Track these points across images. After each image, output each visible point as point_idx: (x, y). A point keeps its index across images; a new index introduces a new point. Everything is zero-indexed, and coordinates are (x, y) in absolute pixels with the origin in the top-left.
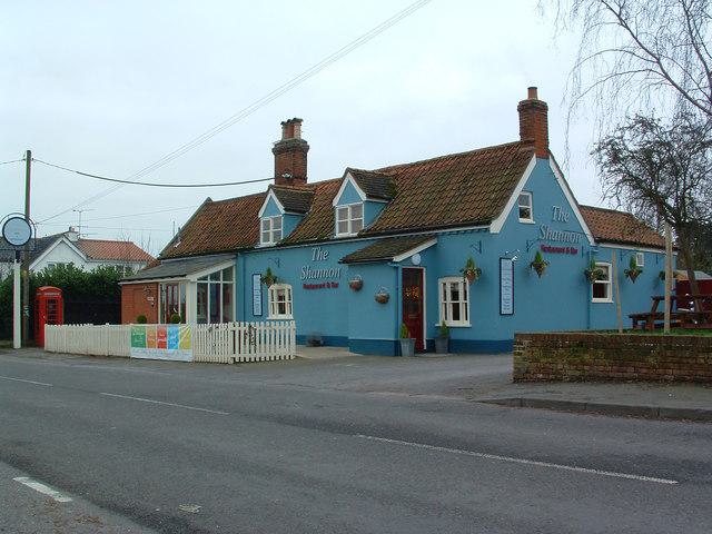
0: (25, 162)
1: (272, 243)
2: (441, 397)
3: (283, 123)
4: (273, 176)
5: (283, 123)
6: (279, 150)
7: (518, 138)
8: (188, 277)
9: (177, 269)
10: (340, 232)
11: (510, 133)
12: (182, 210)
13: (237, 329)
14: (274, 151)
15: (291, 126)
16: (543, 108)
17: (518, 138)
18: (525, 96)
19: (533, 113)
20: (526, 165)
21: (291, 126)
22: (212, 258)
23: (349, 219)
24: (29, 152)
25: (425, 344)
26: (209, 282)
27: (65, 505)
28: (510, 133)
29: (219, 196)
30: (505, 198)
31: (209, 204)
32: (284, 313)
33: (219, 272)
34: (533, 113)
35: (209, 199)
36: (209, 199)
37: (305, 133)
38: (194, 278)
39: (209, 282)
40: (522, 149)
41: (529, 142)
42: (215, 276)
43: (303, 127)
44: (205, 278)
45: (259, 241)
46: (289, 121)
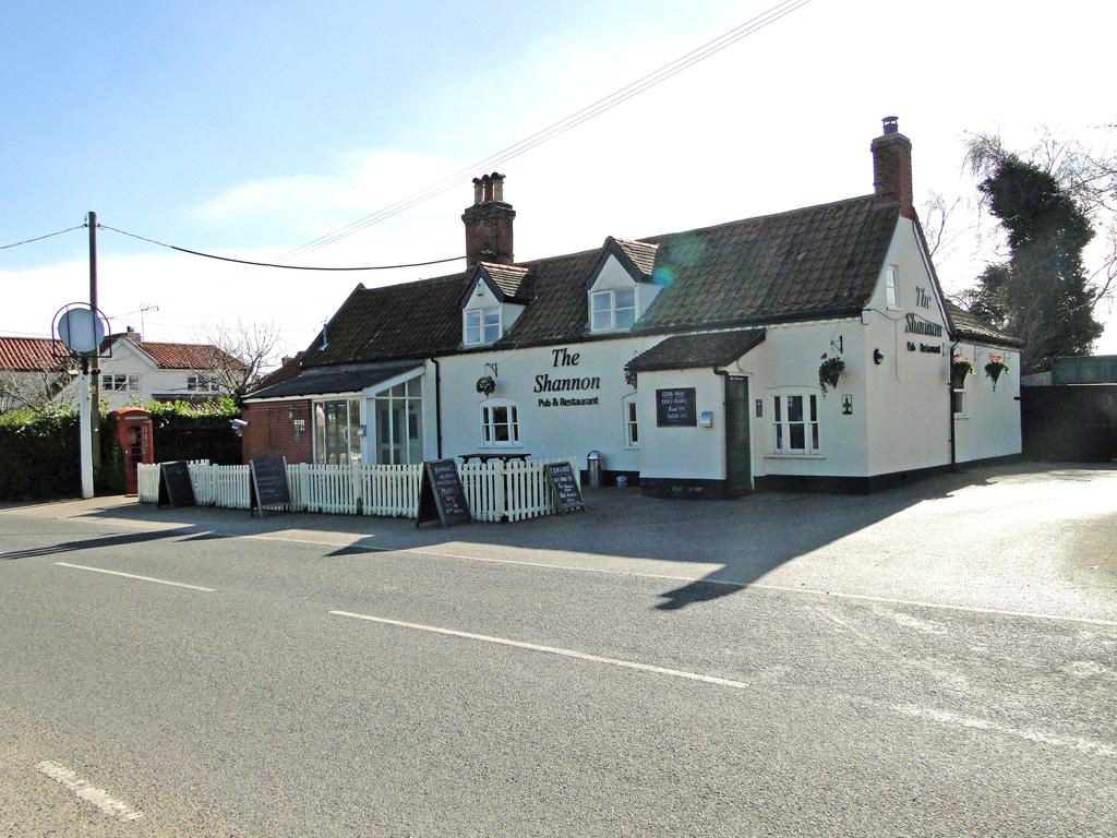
0: (87, 230)
3: (475, 180)
4: (463, 252)
5: (475, 180)
6: (470, 217)
11: (859, 182)
12: (330, 299)
14: (872, 150)
15: (489, 183)
16: (905, 145)
18: (880, 133)
19: (891, 155)
21: (489, 183)
23: (613, 308)
24: (92, 215)
25: (753, 482)
26: (391, 398)
27: (59, 757)
28: (859, 182)
29: (374, 281)
31: (360, 293)
32: (505, 438)
34: (891, 155)
35: (361, 285)
36: (361, 285)
37: (509, 194)
39: (391, 398)
40: (881, 206)
42: (399, 390)
43: (507, 185)
44: (385, 393)
46: (485, 177)
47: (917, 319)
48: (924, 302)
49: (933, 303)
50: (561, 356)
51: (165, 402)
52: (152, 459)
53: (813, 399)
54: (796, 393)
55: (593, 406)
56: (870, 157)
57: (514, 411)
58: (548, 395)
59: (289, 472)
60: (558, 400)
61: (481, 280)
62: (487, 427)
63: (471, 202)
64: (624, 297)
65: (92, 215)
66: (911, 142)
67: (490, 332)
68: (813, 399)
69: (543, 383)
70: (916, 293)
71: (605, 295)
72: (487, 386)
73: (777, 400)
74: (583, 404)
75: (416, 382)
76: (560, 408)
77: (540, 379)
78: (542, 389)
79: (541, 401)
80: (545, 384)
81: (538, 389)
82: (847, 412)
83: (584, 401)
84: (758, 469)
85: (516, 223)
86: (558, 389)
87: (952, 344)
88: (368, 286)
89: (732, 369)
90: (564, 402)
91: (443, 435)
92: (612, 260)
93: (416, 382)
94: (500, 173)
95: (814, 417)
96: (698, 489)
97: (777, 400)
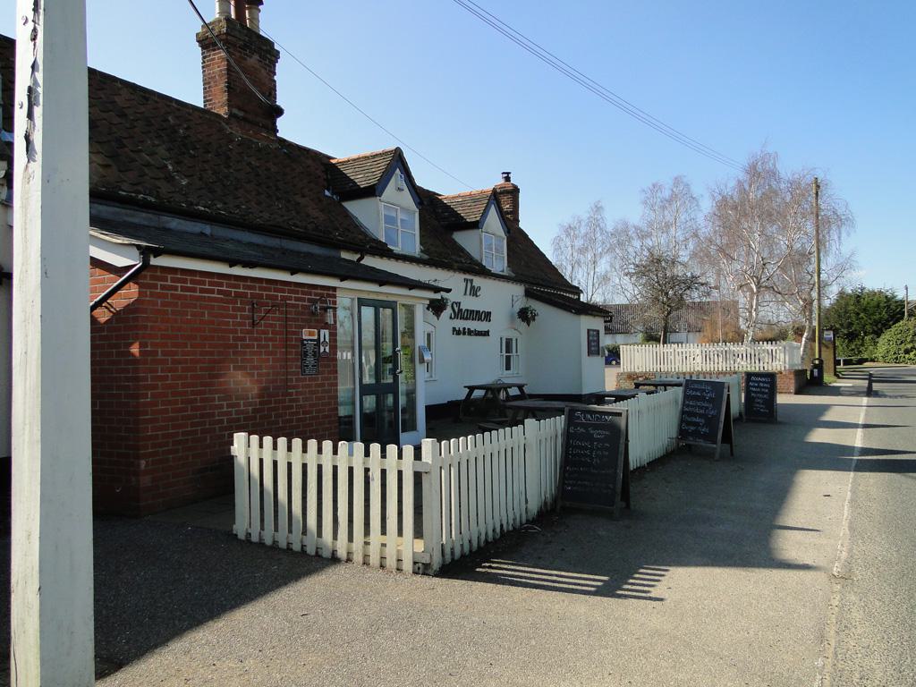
90: (470, 332)
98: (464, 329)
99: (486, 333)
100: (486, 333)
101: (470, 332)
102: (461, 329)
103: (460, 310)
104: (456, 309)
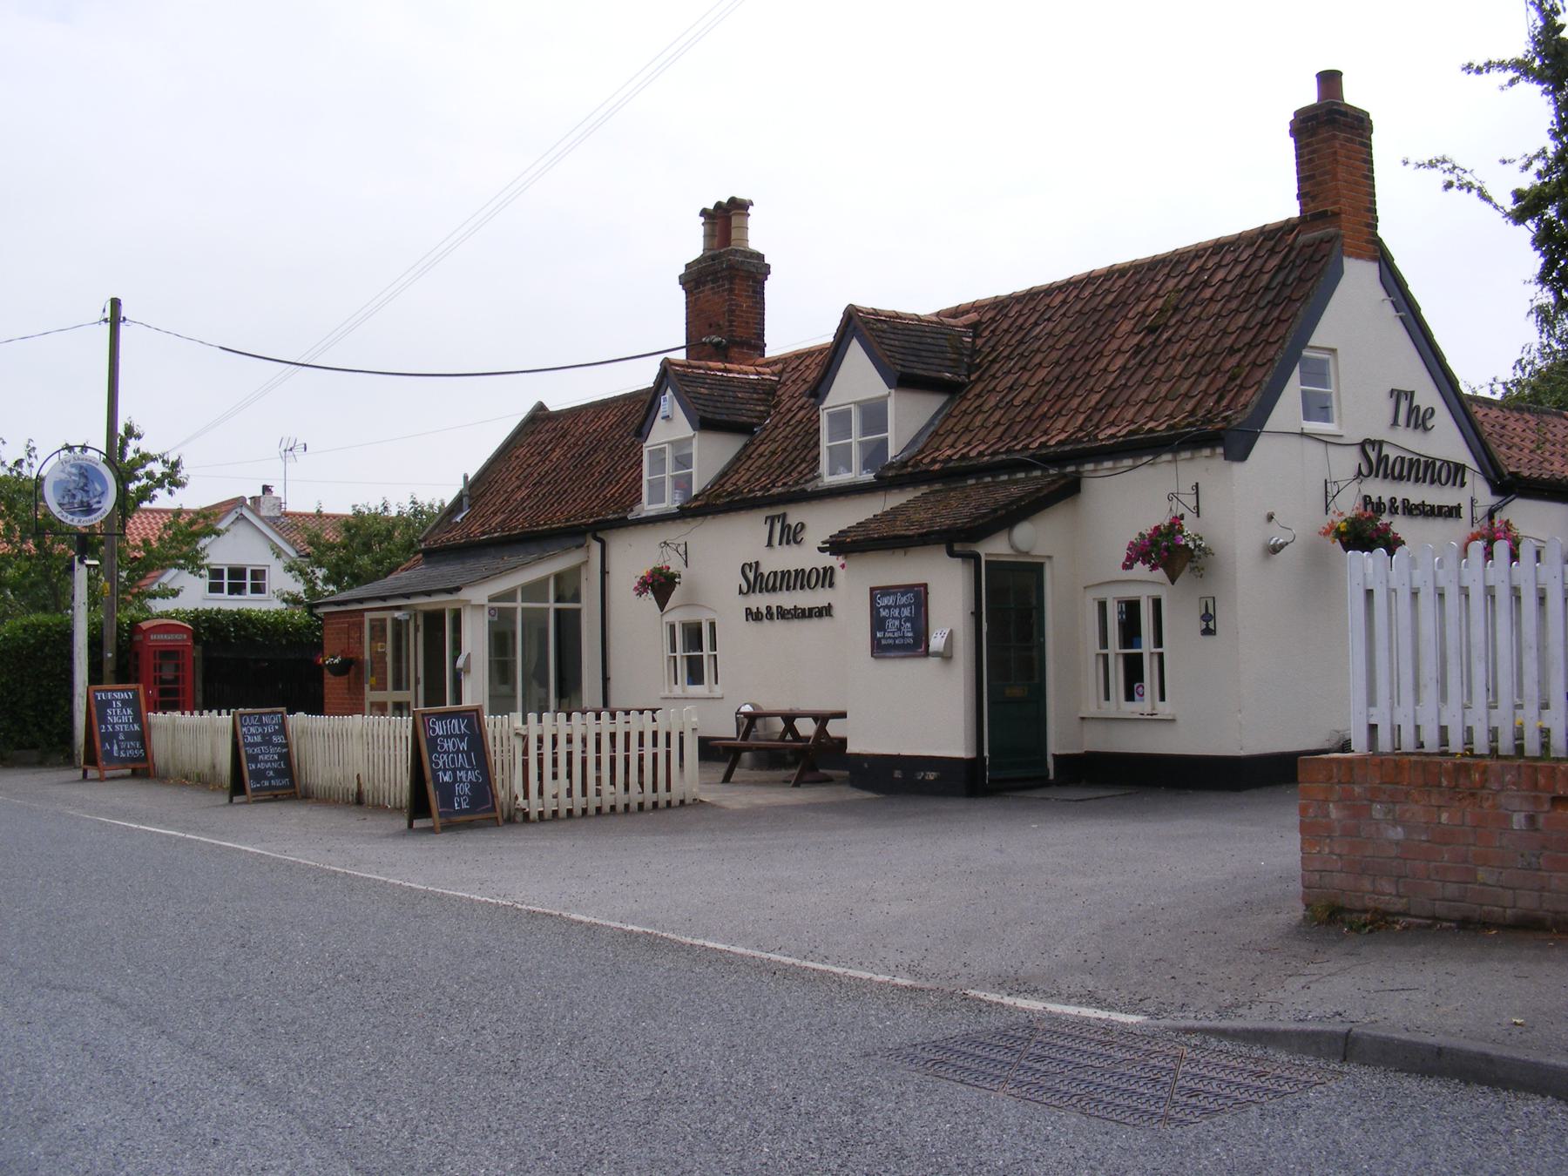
1: (856, 474)
2: (1008, 1000)
5: (704, 213)
6: (695, 279)
7: (1292, 210)
8: (465, 594)
9: (447, 572)
10: (832, 473)
13: (533, 730)
16: (1359, 124)
17: (1292, 210)
20: (843, 770)
22: (485, 563)
23: (856, 438)
24: (116, 304)
29: (563, 395)
30: (234, 849)
31: (539, 418)
33: (545, 580)
35: (541, 407)
36: (541, 407)
37: (758, 236)
38: (479, 595)
39: (519, 605)
41: (1323, 215)
42: (533, 591)
44: (509, 595)
45: (639, 499)
46: (719, 205)
47: (1392, 454)
48: (1419, 420)
49: (1443, 420)
50: (778, 527)
51: (4, 621)
52: (199, 699)
53: (1157, 604)
54: (1130, 593)
55: (826, 620)
56: (1286, 149)
57: (713, 625)
58: (760, 601)
59: (489, 731)
60: (775, 610)
61: (669, 392)
62: (1106, 657)
63: (1521, 57)
64: (874, 415)
65: (116, 304)
66: (1288, 128)
67: (683, 483)
68: (1157, 604)
69: (751, 576)
70: (1391, 403)
71: (660, 450)
72: (660, 585)
73: (1102, 606)
74: (810, 616)
75: (576, 571)
76: (779, 625)
77: (1369, 449)
78: (751, 588)
79: (748, 612)
80: (756, 580)
81: (745, 588)
82: (1208, 632)
83: (811, 610)
84: (1060, 739)
85: (771, 287)
86: (774, 589)
87: (1494, 500)
88: (553, 406)
89: (995, 548)
90: (783, 614)
91: (613, 673)
92: (856, 357)
93: (576, 571)
94: (740, 195)
95: (1159, 642)
96: (931, 776)
97: (1102, 606)
98: (1393, 500)
99: (825, 611)
100: (825, 611)
101: (783, 614)
102: (1385, 500)
103: (1383, 459)
104: (1373, 456)
